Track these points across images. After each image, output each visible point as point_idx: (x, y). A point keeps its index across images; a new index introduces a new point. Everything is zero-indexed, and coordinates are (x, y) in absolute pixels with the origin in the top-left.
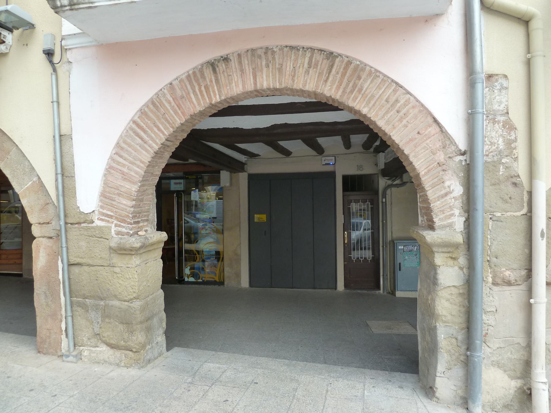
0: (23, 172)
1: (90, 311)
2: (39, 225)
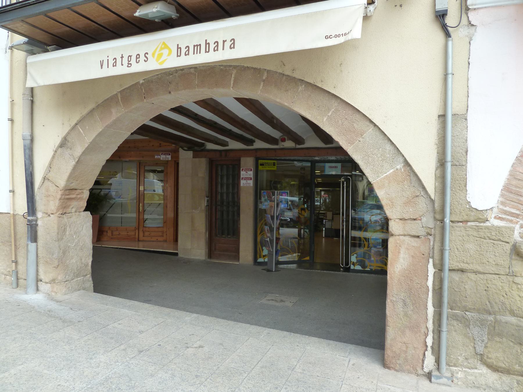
0: (381, 158)
1: (471, 327)
2: (400, 221)
